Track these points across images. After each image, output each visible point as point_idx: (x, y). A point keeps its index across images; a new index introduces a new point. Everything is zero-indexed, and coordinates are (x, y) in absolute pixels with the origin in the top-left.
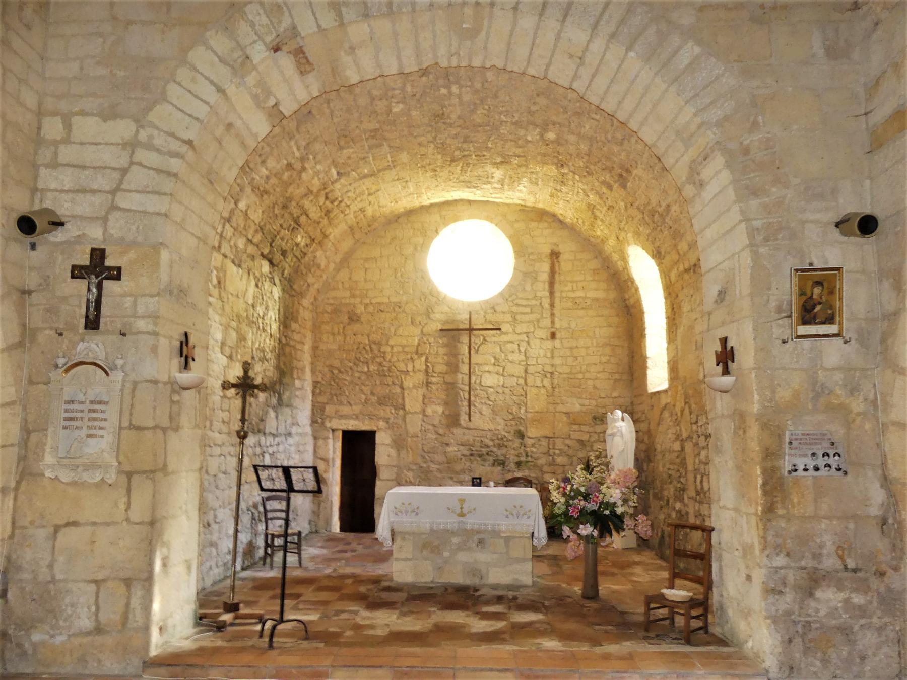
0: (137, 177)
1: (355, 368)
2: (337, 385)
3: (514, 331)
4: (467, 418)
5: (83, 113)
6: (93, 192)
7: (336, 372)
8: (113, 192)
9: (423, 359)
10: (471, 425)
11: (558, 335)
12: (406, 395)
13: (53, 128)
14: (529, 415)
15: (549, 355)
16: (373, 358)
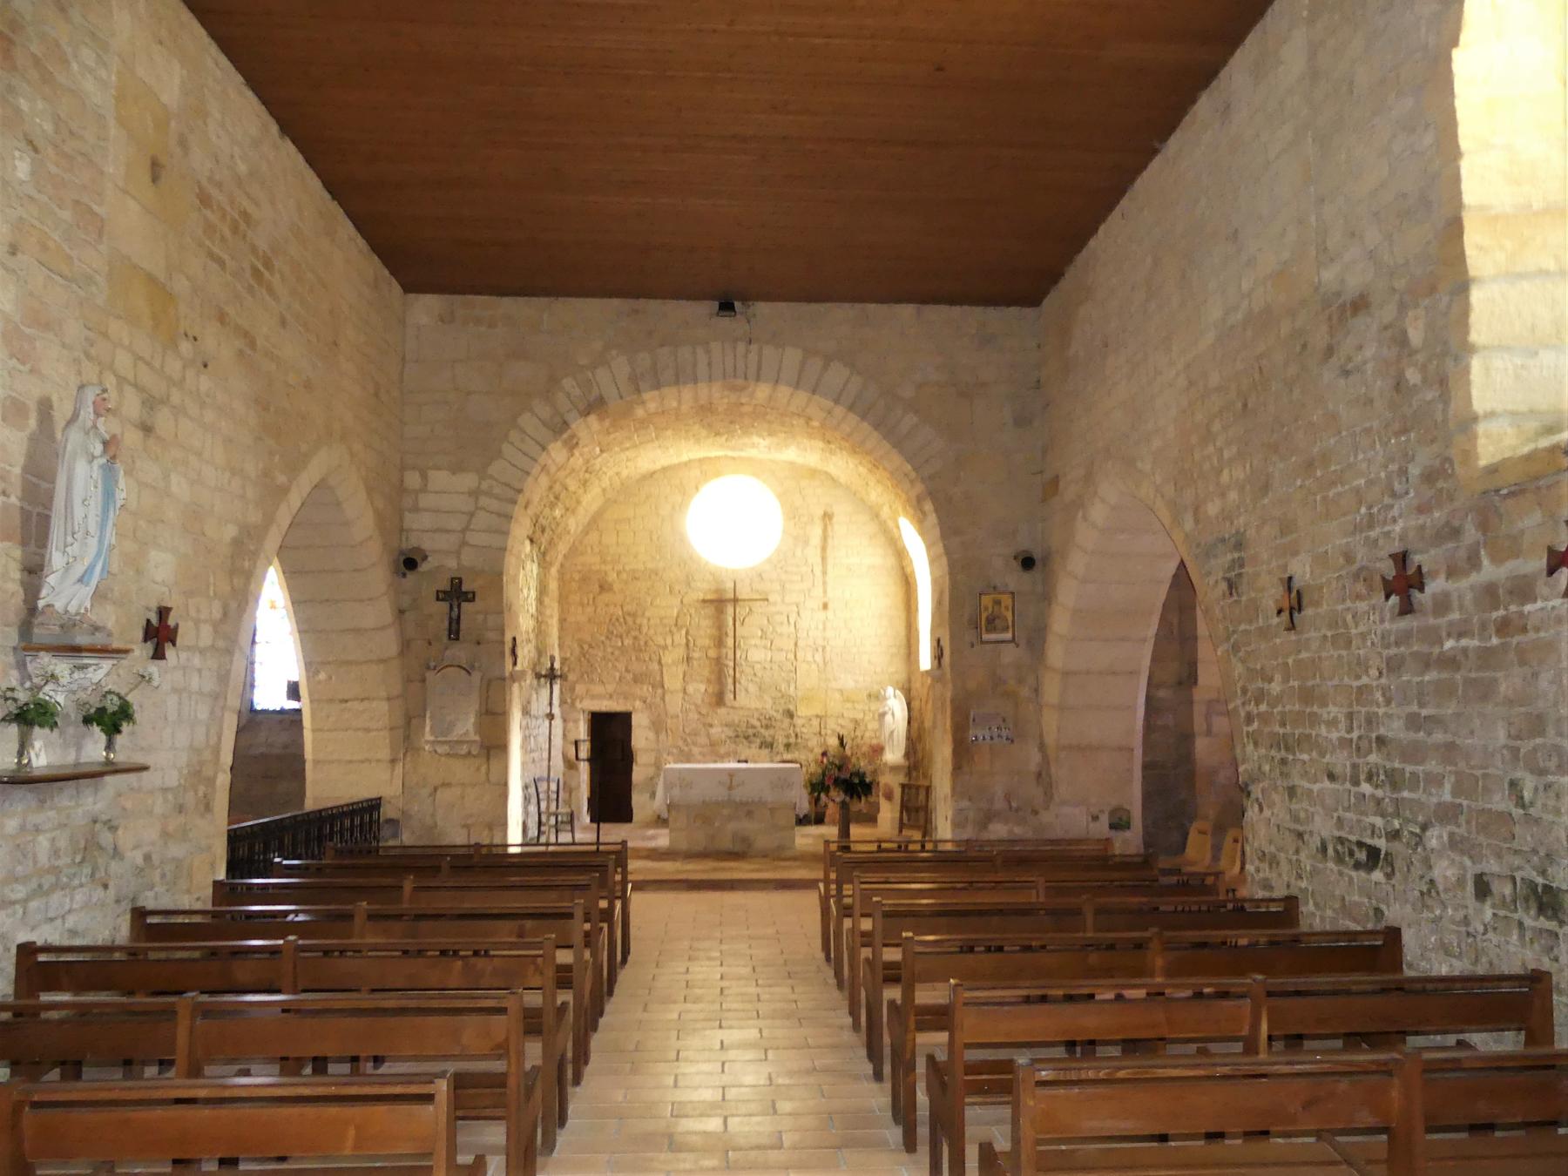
0: (482, 519)
1: (608, 642)
2: (588, 661)
3: (783, 601)
4: (732, 696)
5: (438, 468)
6: (448, 531)
7: (586, 647)
8: (464, 531)
9: (684, 632)
10: (736, 704)
11: (830, 606)
12: (665, 672)
13: (412, 479)
14: (800, 694)
15: (821, 627)
16: (628, 633)
